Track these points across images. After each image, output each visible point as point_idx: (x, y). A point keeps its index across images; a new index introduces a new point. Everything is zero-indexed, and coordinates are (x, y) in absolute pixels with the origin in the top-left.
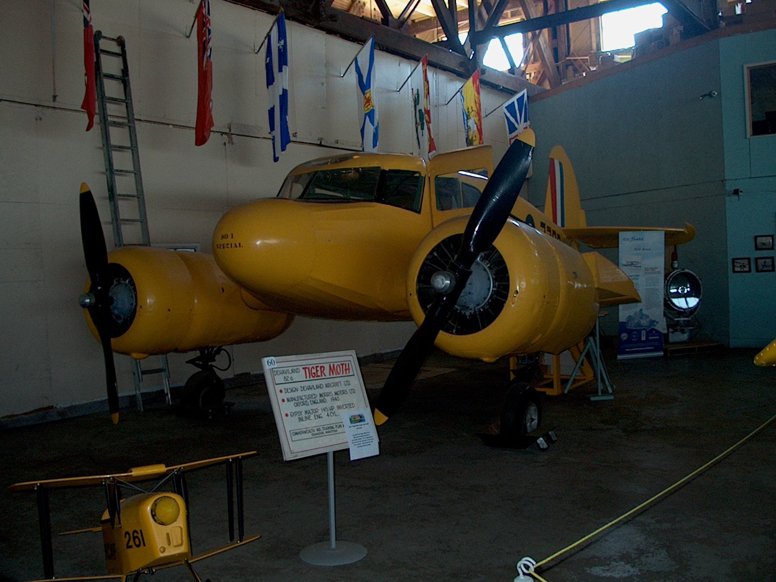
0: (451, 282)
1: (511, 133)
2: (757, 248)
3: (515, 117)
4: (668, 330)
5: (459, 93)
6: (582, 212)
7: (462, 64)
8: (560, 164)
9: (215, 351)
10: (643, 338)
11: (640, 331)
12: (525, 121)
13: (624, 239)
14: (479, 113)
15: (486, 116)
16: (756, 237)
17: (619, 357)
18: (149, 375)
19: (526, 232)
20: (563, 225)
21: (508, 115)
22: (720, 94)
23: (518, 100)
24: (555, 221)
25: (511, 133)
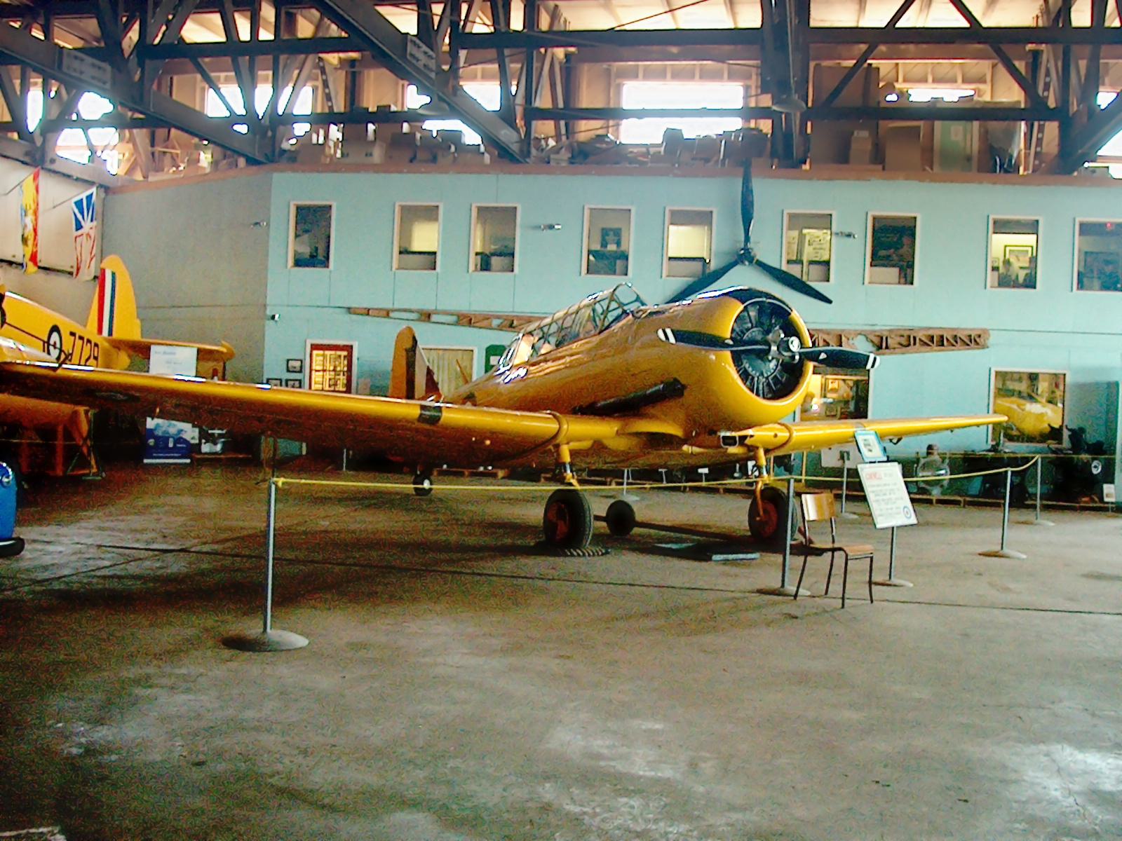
0: (1023, 109)
1: (77, 230)
2: (288, 371)
3: (82, 214)
4: (200, 441)
5: (19, 187)
6: (138, 322)
7: (27, 154)
8: (113, 274)
9: (28, 833)
10: (171, 445)
11: (168, 439)
12: (92, 220)
13: (156, 353)
14: (36, 213)
15: (54, 207)
16: (1006, 246)
17: (146, 461)
18: (694, 346)
19: (641, 156)
20: (110, 333)
21: (76, 211)
22: (268, 225)
23: (87, 197)
24: (100, 331)
25: (77, 230)
